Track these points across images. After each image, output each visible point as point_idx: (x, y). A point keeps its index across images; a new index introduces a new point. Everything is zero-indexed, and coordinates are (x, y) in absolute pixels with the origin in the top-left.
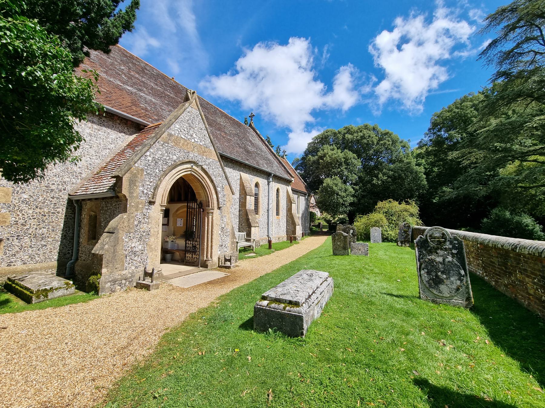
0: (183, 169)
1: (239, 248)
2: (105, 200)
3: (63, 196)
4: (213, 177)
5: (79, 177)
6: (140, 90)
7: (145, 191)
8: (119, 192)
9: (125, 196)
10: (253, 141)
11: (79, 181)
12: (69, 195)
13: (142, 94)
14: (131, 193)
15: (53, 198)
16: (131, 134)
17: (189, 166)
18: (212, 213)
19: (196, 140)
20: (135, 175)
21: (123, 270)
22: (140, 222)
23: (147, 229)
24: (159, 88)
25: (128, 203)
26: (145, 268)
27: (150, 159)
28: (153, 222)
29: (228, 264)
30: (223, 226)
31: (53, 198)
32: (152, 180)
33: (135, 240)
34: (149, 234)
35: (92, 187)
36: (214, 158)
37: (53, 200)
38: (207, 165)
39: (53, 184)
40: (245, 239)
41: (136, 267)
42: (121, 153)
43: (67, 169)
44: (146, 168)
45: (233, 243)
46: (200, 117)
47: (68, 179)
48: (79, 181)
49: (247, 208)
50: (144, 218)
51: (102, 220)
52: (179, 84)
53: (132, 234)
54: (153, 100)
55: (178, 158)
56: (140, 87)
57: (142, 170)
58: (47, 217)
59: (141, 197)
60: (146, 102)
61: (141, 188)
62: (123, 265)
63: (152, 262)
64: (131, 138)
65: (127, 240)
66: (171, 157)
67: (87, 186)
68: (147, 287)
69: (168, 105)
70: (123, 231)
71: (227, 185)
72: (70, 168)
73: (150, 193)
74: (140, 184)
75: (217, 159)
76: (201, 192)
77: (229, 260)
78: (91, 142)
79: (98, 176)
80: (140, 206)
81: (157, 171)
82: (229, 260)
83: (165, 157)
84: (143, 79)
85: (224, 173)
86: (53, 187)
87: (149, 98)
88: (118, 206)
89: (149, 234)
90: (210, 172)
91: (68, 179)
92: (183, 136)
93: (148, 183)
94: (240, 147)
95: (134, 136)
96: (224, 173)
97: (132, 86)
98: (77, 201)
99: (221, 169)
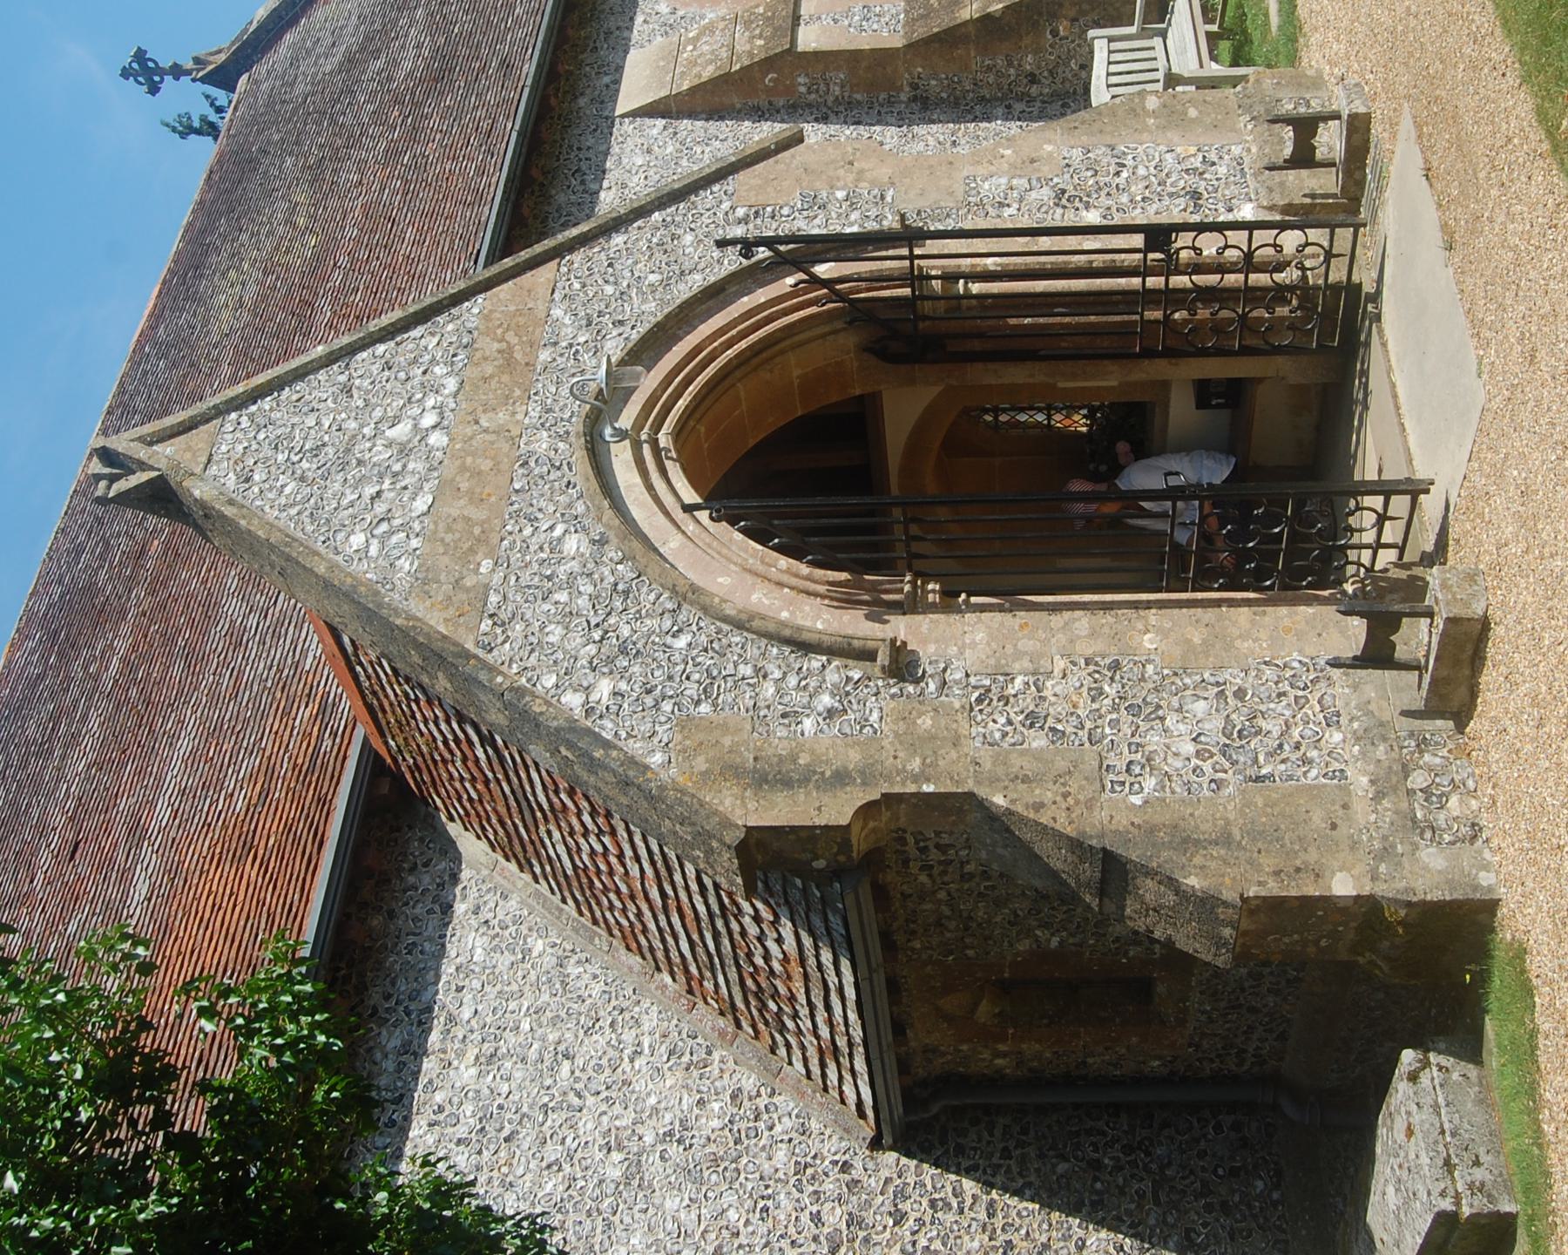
0: (650, 488)
1: (1215, 69)
2: (900, 938)
3: (885, 1173)
4: (684, 290)
5: (762, 1102)
6: (137, 833)
7: (826, 700)
8: (845, 845)
9: (867, 811)
10: (350, 41)
11: (783, 1101)
12: (876, 1144)
13: (163, 812)
14: (841, 778)
15: (899, 1218)
16: (449, 850)
17: (621, 458)
18: (950, 278)
19: (429, 420)
20: (731, 771)
21: (1345, 790)
22: (1032, 720)
23: (1080, 676)
24: (94, 723)
25: (911, 788)
26: (1335, 663)
27: (603, 689)
28: (1026, 645)
29: (1330, 141)
30: (1046, 194)
31: (899, 1218)
32: (747, 670)
33: (1154, 740)
34: (1116, 666)
35: (821, 1016)
36: (543, 292)
37: (913, 1216)
38: (600, 335)
39: (817, 1218)
40: (1143, 34)
41: (1332, 721)
42: (581, 887)
43: (716, 1160)
44: (667, 706)
45: (1172, 117)
46: (267, 403)
47: (781, 1154)
48: (783, 1101)
49: (898, 42)
50: (1005, 700)
51: (1024, 946)
52: (29, 615)
53: (1111, 759)
54: (184, 745)
55: (576, 524)
56: (119, 831)
57: (685, 724)
58: (1015, 1238)
59: (863, 722)
60: (212, 785)
61: (808, 724)
62: (1313, 791)
63: (1300, 636)
64: (470, 846)
65: (1150, 783)
66: (574, 566)
67: (812, 1053)
68: (1467, 644)
69: (194, 659)
70: (1090, 804)
71: (731, 183)
72: (712, 1148)
73: (832, 677)
74: (782, 732)
75: (546, 272)
76: (795, 367)
77: (1305, 127)
78: (533, 1054)
79: (756, 1008)
80: (926, 722)
81: (681, 642)
82: (1305, 127)
83: (583, 602)
84: (59, 820)
85: (641, 212)
86: (835, 1217)
87: (175, 775)
88: (934, 855)
89: (1116, 666)
90: (651, 311)
91: (781, 1154)
92: (421, 504)
93: (769, 690)
94: (414, 134)
95: (454, 829)
96: (641, 212)
97: (126, 876)
98: (910, 1099)
99: (618, 239)
